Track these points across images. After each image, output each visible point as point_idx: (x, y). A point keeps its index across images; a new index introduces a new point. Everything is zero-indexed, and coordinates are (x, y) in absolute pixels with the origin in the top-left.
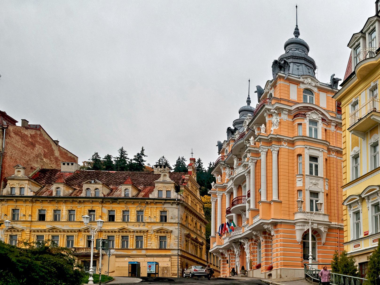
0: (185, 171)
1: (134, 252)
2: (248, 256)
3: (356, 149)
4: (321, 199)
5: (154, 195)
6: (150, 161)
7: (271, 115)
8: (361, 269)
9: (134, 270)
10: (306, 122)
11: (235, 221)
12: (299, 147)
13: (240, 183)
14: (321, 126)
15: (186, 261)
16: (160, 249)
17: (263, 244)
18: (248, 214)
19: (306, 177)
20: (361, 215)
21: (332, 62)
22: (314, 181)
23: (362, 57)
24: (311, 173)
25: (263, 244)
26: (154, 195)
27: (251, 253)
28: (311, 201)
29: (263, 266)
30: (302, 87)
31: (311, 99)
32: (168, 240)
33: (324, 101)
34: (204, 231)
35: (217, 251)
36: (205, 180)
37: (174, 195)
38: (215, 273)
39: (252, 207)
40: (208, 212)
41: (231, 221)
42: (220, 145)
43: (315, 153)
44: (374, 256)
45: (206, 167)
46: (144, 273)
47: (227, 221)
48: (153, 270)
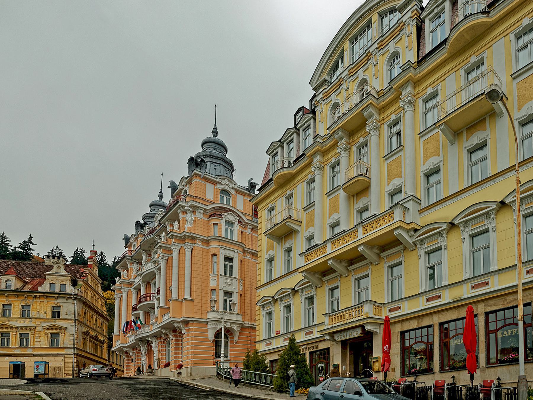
0: (85, 263)
1: (18, 351)
2: (156, 354)
3: (271, 252)
4: (235, 298)
5: (45, 288)
6: (39, 251)
7: (185, 212)
8: (272, 366)
9: (17, 370)
10: (222, 222)
11: (142, 318)
12: (214, 247)
13: (149, 280)
14: (237, 228)
15: (83, 360)
16: (52, 347)
17: (173, 343)
18: (157, 312)
19: (220, 277)
20: (274, 315)
21: (250, 166)
22: (228, 281)
23: (279, 166)
24: (226, 273)
25: (173, 343)
26: (45, 288)
27: (159, 351)
28: (225, 301)
29: (172, 365)
30: (219, 187)
31: (228, 201)
32: (61, 338)
33: (241, 204)
34: (105, 328)
35: (120, 349)
36: (108, 275)
37: (70, 289)
38: (118, 373)
39: (162, 304)
40: (111, 309)
41: (138, 318)
42: (127, 240)
43: (230, 254)
44: (285, 354)
45: (109, 261)
46: (30, 373)
47: (133, 318)
48: (42, 370)
